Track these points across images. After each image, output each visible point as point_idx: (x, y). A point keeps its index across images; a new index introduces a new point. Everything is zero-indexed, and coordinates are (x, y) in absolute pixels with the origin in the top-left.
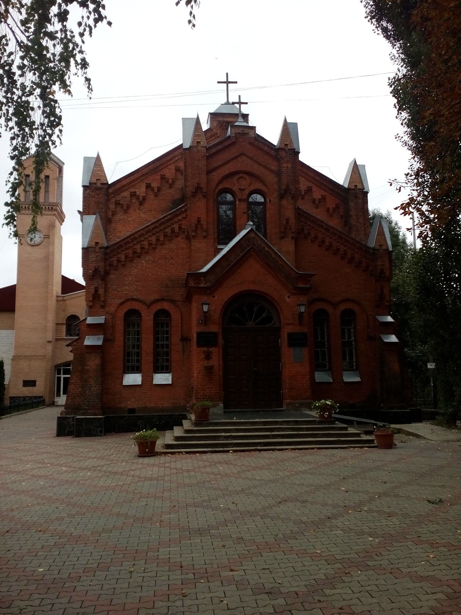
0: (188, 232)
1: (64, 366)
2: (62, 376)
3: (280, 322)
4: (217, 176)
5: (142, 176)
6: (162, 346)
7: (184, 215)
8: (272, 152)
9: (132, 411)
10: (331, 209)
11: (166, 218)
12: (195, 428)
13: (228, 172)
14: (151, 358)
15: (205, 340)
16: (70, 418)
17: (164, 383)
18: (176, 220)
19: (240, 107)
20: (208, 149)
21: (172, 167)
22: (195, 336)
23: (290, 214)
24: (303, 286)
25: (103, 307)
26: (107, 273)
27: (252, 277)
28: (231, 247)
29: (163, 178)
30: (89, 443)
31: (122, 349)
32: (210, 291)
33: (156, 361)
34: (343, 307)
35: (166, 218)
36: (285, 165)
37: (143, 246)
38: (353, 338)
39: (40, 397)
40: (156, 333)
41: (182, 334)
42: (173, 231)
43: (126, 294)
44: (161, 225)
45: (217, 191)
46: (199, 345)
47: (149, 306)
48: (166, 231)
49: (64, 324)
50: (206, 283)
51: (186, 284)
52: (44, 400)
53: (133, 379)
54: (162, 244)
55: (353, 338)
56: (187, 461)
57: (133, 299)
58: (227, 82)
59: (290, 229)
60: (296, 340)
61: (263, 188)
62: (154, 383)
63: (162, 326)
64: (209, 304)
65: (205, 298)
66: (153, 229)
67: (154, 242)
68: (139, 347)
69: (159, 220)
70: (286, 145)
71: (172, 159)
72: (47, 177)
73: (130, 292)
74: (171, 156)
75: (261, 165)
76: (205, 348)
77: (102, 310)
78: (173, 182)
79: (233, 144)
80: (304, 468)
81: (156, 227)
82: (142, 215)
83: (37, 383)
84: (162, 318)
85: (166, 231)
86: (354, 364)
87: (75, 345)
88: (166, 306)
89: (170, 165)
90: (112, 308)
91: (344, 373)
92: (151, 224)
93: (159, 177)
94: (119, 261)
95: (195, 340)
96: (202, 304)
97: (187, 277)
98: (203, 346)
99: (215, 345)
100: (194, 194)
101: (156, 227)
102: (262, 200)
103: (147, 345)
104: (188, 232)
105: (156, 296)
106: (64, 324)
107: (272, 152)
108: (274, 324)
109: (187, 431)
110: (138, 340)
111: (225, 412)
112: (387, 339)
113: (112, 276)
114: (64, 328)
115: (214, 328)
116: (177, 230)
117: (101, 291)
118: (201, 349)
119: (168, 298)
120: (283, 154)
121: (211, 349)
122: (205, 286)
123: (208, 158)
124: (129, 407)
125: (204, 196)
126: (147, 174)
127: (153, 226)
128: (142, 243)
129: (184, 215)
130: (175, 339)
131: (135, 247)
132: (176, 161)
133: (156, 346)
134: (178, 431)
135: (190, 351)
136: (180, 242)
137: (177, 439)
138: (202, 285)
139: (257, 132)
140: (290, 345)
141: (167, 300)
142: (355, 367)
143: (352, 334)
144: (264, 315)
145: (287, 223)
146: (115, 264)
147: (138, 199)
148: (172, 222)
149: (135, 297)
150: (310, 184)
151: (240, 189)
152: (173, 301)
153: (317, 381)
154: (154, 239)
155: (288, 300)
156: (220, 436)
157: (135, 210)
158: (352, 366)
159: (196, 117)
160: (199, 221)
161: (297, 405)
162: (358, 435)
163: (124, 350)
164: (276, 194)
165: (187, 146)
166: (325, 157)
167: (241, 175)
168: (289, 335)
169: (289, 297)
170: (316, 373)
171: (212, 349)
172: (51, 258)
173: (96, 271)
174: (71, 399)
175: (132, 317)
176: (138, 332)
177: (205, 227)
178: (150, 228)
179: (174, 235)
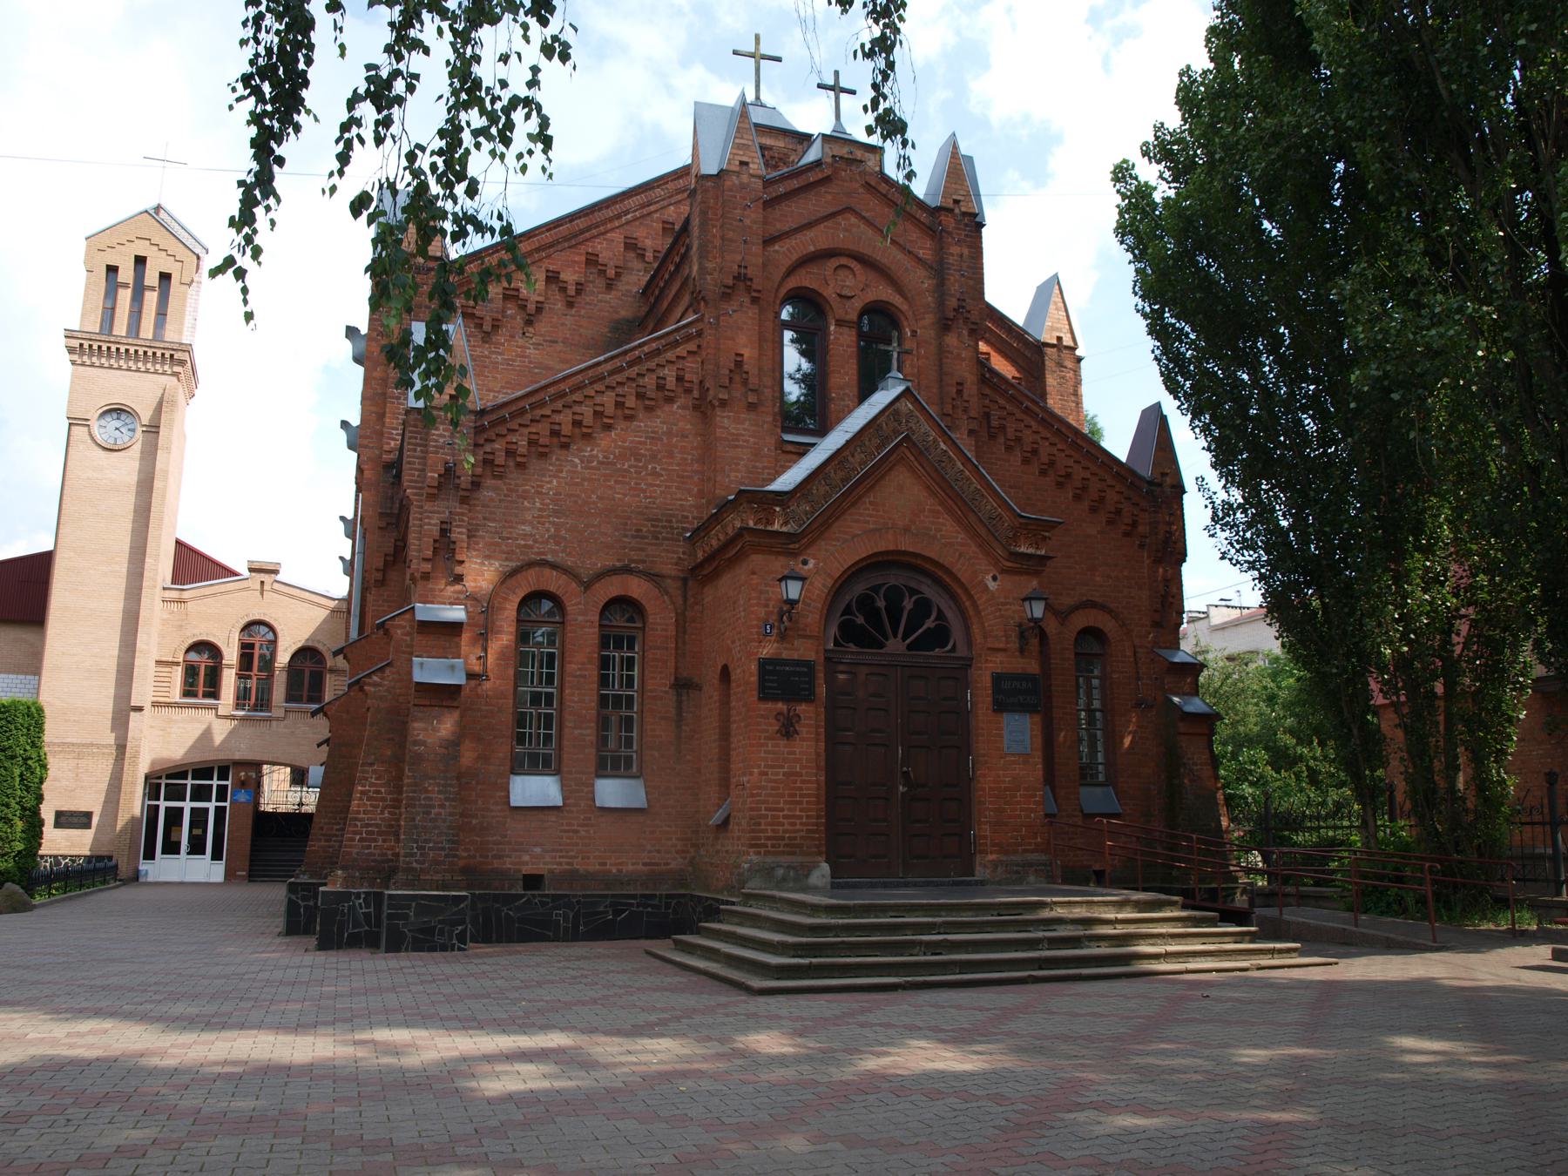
1: (168, 777)
2: (163, 804)
4: (788, 252)
5: (538, 250)
6: (617, 699)
7: (692, 346)
8: (923, 217)
9: (533, 881)
11: (646, 349)
13: (812, 249)
14: (589, 733)
15: (781, 682)
16: (358, 896)
18: (670, 355)
20: (768, 183)
21: (617, 237)
23: (965, 371)
24: (1031, 551)
26: (476, 485)
27: (903, 514)
28: (857, 428)
29: (592, 260)
32: (790, 545)
34: (1080, 621)
35: (646, 349)
36: (955, 250)
37: (577, 418)
39: (110, 858)
41: (676, 669)
43: (525, 546)
44: (631, 364)
45: (783, 291)
46: (765, 694)
47: (587, 586)
48: (641, 381)
49: (177, 664)
50: (786, 523)
52: (116, 866)
57: (544, 563)
58: (758, 57)
59: (965, 410)
60: (1013, 694)
64: (803, 579)
66: (612, 373)
70: (956, 202)
71: (619, 217)
72: (165, 277)
73: (535, 541)
74: (632, 202)
76: (780, 705)
78: (618, 275)
79: (827, 180)
81: (620, 370)
82: (531, 351)
85: (641, 381)
88: (636, 588)
89: (612, 230)
93: (583, 258)
98: (775, 699)
99: (809, 697)
100: (727, 294)
101: (620, 370)
103: (580, 695)
105: (611, 561)
106: (177, 664)
107: (923, 217)
108: (953, 649)
111: (834, 886)
113: (486, 494)
114: (178, 674)
115: (802, 650)
116: (671, 382)
118: (770, 705)
119: (641, 567)
120: (948, 222)
122: (784, 529)
123: (769, 204)
124: (527, 870)
125: (755, 300)
126: (551, 245)
127: (609, 366)
128: (577, 409)
129: (692, 346)
131: (557, 418)
132: (628, 223)
136: (676, 417)
138: (776, 527)
140: (1000, 707)
141: (639, 573)
142: (1101, 778)
144: (929, 623)
145: (959, 392)
147: (523, 308)
148: (660, 360)
149: (549, 558)
151: (840, 296)
152: (654, 577)
154: (608, 399)
155: (992, 585)
157: (512, 336)
160: (739, 364)
164: (929, 319)
165: (710, 167)
167: (844, 261)
168: (997, 679)
169: (994, 578)
171: (802, 708)
172: (157, 484)
174: (361, 840)
177: (753, 380)
178: (600, 369)
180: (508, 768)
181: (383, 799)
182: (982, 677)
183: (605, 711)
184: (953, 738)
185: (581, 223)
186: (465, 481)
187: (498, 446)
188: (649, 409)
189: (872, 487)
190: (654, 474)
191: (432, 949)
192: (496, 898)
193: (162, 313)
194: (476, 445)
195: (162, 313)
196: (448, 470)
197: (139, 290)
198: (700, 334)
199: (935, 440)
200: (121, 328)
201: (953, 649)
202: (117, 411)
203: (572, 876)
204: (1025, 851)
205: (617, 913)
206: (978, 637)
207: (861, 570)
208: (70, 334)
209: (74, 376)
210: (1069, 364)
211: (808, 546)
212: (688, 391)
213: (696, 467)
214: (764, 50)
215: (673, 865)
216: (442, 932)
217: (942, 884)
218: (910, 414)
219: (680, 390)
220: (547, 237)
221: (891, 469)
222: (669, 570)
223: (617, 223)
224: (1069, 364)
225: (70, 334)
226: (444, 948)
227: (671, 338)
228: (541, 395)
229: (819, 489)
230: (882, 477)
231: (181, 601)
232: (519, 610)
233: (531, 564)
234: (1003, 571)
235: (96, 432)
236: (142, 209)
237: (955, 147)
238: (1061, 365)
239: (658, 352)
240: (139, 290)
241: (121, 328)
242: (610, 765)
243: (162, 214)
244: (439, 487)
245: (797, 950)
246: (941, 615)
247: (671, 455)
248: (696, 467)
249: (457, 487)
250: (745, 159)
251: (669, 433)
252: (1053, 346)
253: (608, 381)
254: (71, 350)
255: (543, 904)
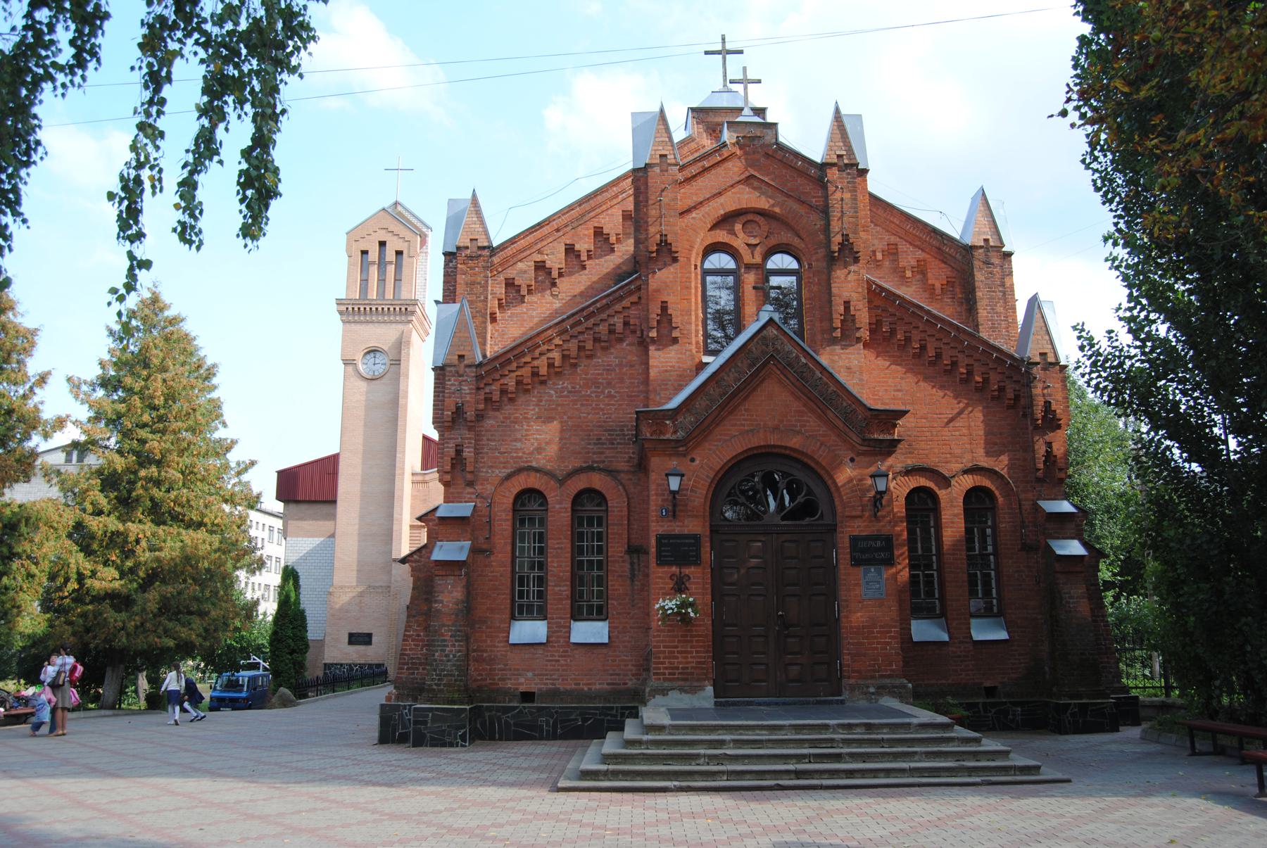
0: (642, 331)
3: (834, 513)
7: (634, 298)
9: (528, 696)
10: (938, 286)
11: (598, 305)
12: (645, 738)
14: (565, 589)
16: (405, 707)
17: (592, 641)
18: (618, 307)
19: (746, 88)
22: (653, 541)
25: (470, 484)
26: (480, 417)
30: (433, 761)
31: (509, 569)
32: (682, 448)
33: (576, 597)
35: (598, 305)
38: (990, 549)
39: (379, 666)
40: (577, 537)
41: (629, 539)
42: (611, 332)
44: (587, 318)
48: (597, 329)
50: (675, 432)
51: (636, 436)
53: (529, 631)
54: (590, 357)
55: (990, 549)
56: (623, 808)
57: (531, 469)
61: (796, 241)
62: (573, 640)
63: (590, 524)
64: (682, 475)
65: (673, 463)
67: (574, 353)
68: (541, 566)
69: (582, 310)
71: (616, 196)
75: (789, 196)
77: (469, 490)
80: (880, 832)
83: (374, 639)
84: (587, 502)
85: (597, 329)
86: (995, 601)
87: (416, 561)
88: (597, 481)
90: (489, 487)
91: (973, 621)
92: (568, 317)
94: (503, 392)
95: (654, 550)
96: (667, 475)
97: (637, 419)
98: (670, 564)
99: (696, 561)
101: (579, 323)
102: (794, 265)
103: (559, 563)
104: (642, 331)
105: (578, 463)
108: (822, 516)
109: (630, 743)
110: (541, 551)
112: (1062, 548)
113: (489, 423)
115: (693, 526)
116: (619, 327)
117: (468, 453)
118: (666, 569)
121: (687, 571)
122: (674, 437)
124: (522, 689)
129: (634, 298)
130: (616, 549)
133: (577, 566)
134: (611, 744)
135: (647, 575)
137: (606, 758)
138: (668, 436)
139: (781, 139)
140: (857, 562)
142: (995, 609)
143: (989, 540)
146: (496, 397)
148: (611, 311)
149: (534, 464)
150: (893, 239)
152: (610, 472)
153: (915, 639)
156: (697, 756)
158: (991, 609)
159: (657, 109)
161: (872, 690)
162: (1005, 754)
163: (513, 571)
166: (917, 177)
167: (750, 217)
170: (914, 623)
173: (459, 411)
175: (528, 502)
176: (541, 534)
179: (615, 337)
180: (508, 616)
181: (423, 640)
182: (843, 540)
183: (581, 573)
184: (824, 588)
185: (586, 206)
186: (470, 414)
187: (495, 387)
188: (605, 349)
189: (747, 396)
190: (610, 396)
191: (443, 745)
192: (498, 709)
193: (397, 280)
194: (478, 389)
195: (397, 280)
196: (458, 408)
197: (382, 263)
198: (639, 288)
199: (797, 357)
200: (373, 294)
201: (822, 516)
202: (373, 351)
203: (554, 694)
204: (882, 676)
205: (585, 720)
206: (839, 509)
207: (755, 456)
208: (339, 302)
209: (344, 331)
210: (996, 261)
211: (695, 448)
212: (634, 332)
213: (641, 388)
214: (728, 47)
215: (630, 684)
216: (449, 735)
217: (808, 703)
218: (776, 338)
219: (628, 332)
220: (565, 219)
221: (762, 382)
222: (623, 466)
223: (615, 201)
224: (996, 261)
225: (339, 302)
226: (451, 745)
227: (617, 295)
228: (523, 348)
229: (700, 404)
230: (754, 389)
231: (425, 482)
232: (515, 503)
233: (520, 470)
234: (859, 454)
235: (361, 367)
236: (381, 207)
237: (837, 111)
238: (987, 263)
239: (607, 306)
240: (382, 263)
241: (373, 294)
242: (578, 614)
243: (400, 208)
244: (453, 421)
245: (814, 743)
246: (810, 492)
247: (622, 381)
248: (641, 388)
249: (465, 420)
250: (664, 152)
251: (620, 365)
252: (981, 247)
253: (571, 332)
254: (341, 313)
255: (532, 714)
